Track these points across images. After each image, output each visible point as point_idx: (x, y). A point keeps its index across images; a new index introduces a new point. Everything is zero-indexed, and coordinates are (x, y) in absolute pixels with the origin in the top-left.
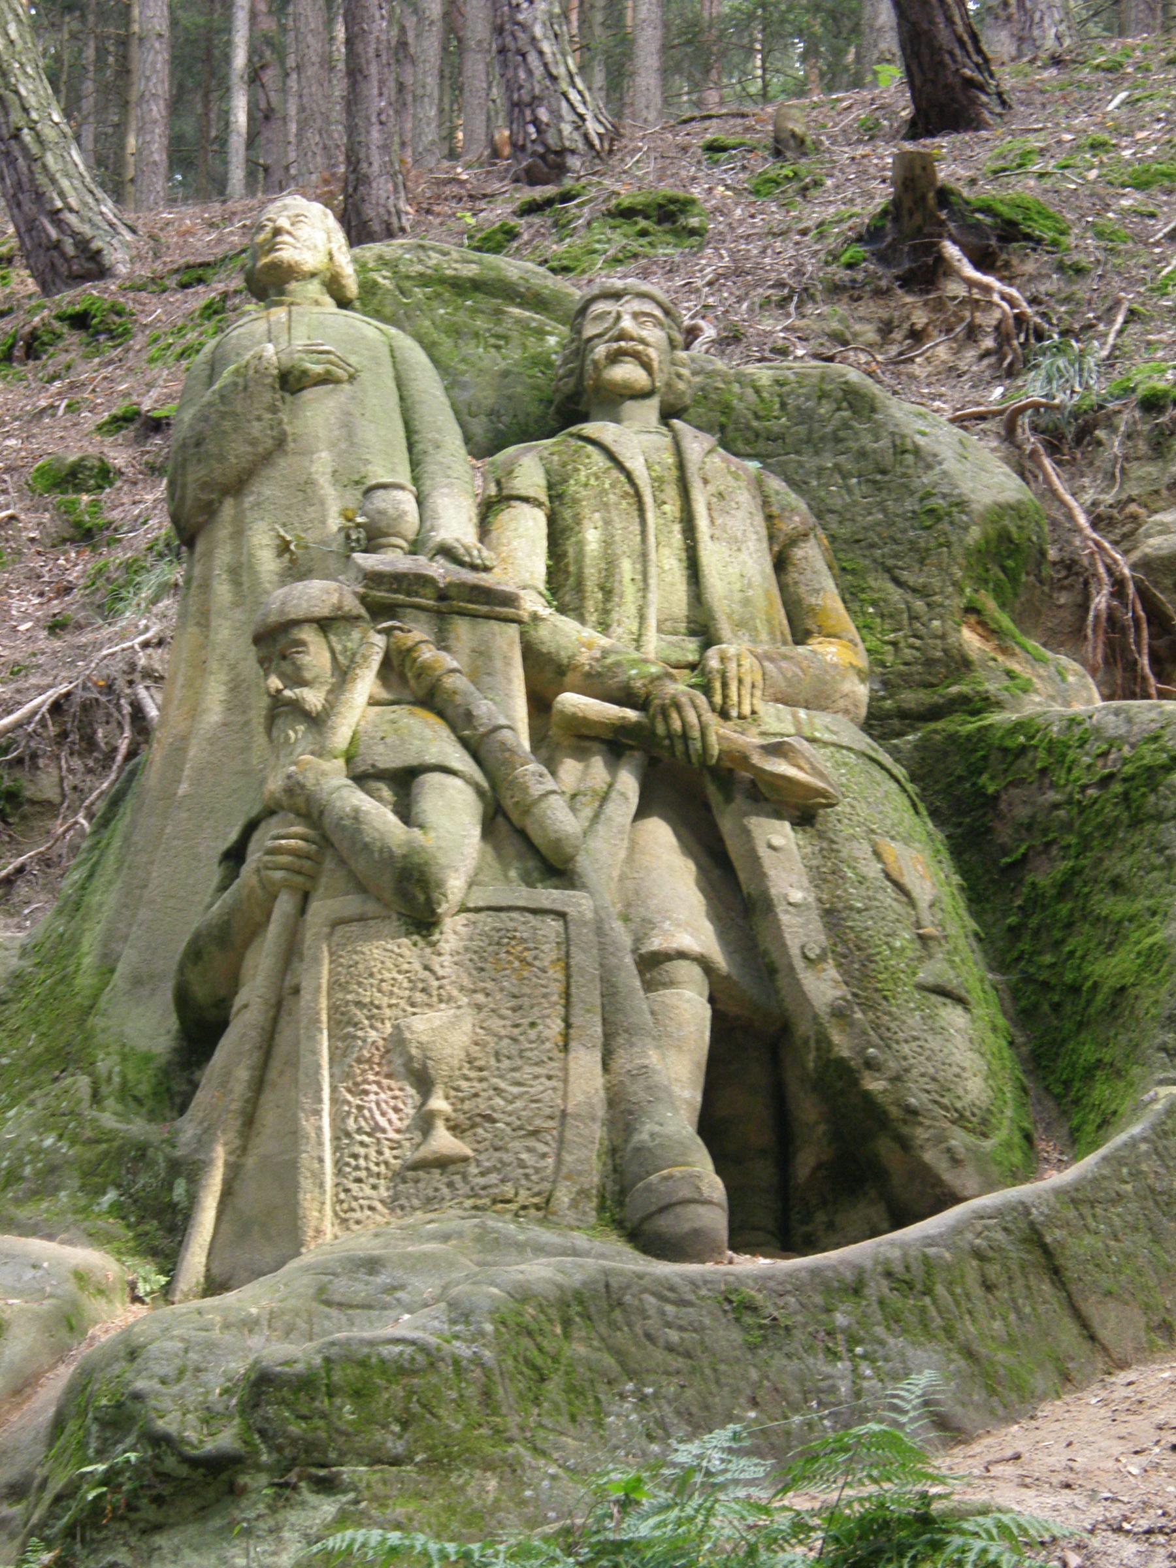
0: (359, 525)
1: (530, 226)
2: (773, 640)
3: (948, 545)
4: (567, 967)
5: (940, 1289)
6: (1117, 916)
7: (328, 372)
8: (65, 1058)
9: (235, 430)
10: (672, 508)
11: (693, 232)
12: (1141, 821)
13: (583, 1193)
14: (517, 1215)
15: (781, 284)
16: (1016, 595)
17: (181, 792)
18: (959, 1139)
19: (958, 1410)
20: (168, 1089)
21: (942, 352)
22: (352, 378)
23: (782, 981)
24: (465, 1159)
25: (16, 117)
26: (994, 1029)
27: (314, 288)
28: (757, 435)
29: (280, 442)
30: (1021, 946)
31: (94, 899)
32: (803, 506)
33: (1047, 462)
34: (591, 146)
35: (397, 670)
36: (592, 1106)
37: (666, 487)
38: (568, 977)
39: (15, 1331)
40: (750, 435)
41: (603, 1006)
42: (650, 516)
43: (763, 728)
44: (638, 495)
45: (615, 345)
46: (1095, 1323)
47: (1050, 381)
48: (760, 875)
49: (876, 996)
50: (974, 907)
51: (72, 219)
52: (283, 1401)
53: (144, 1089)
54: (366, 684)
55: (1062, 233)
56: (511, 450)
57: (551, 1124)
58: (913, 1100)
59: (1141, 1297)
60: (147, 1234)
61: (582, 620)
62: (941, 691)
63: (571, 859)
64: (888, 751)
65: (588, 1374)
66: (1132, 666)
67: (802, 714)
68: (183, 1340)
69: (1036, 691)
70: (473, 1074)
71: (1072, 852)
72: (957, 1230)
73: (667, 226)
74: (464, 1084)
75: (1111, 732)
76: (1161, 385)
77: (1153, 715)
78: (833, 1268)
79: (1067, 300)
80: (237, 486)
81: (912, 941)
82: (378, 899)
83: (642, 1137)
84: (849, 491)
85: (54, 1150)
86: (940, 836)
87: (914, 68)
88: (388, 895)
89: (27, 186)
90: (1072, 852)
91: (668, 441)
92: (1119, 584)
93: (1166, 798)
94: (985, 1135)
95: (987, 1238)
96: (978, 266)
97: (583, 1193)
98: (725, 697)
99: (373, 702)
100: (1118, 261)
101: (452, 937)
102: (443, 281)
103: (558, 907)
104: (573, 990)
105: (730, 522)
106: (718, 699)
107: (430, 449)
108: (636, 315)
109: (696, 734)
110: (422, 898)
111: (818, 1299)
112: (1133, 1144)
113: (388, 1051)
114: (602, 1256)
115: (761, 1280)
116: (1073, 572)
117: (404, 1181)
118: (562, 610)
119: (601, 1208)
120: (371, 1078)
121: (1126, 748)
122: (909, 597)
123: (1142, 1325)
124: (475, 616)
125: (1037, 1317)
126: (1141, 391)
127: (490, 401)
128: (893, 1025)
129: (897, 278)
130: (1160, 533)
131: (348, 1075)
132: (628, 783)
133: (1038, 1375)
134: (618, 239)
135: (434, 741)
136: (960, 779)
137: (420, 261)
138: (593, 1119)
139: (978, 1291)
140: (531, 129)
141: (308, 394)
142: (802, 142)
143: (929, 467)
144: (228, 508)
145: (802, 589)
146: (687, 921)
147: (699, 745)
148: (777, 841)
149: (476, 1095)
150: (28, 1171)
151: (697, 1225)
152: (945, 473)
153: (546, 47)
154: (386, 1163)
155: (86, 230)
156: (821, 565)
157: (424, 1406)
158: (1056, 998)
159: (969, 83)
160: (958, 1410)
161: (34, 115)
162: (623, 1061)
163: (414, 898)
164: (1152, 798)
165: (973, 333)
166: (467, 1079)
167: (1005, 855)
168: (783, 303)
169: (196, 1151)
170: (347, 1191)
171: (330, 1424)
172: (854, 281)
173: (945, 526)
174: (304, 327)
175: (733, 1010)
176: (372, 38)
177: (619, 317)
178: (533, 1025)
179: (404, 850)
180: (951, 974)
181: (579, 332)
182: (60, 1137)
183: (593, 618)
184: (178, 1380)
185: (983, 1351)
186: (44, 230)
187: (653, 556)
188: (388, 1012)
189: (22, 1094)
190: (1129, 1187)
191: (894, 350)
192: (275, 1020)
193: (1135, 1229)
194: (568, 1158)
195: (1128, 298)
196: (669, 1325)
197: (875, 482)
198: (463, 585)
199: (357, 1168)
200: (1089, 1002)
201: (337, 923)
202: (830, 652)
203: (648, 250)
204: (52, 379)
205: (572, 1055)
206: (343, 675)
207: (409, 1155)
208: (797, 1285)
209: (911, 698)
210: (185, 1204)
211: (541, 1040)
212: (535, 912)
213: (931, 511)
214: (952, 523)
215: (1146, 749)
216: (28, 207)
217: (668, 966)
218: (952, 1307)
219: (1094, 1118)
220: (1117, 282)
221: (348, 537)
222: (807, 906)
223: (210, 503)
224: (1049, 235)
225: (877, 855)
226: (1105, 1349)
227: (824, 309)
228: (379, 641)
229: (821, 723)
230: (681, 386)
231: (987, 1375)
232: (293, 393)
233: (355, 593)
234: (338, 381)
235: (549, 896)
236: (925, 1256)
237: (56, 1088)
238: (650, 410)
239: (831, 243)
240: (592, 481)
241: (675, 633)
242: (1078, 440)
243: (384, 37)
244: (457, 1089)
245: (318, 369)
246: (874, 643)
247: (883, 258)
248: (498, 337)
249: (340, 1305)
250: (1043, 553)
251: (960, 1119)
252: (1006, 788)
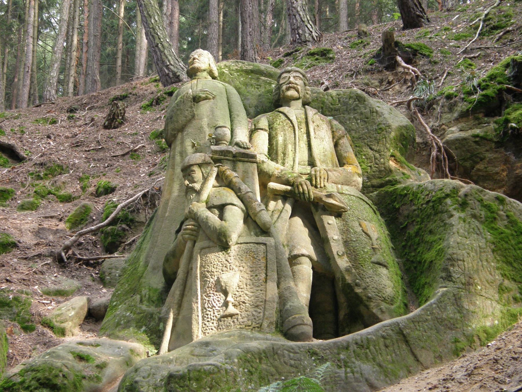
0: (213, 138)
1: (287, 59)
2: (333, 166)
3: (385, 138)
4: (267, 259)
5: (372, 347)
6: (431, 241)
7: (207, 96)
8: (134, 291)
9: (181, 114)
10: (304, 130)
11: (331, 58)
12: (437, 213)
13: (271, 323)
14: (252, 330)
15: (351, 70)
16: (406, 152)
17: (166, 215)
18: (384, 306)
19: (376, 381)
20: (161, 298)
21: (397, 87)
22: (214, 98)
23: (332, 262)
24: (237, 314)
25: (157, 41)
26: (397, 274)
27: (205, 74)
28: (332, 110)
29: (193, 116)
30: (406, 251)
31: (144, 246)
32: (343, 128)
33: (419, 115)
34: (314, 39)
35: (221, 178)
36: (274, 298)
37: (302, 124)
38: (267, 262)
39: (110, 365)
40: (330, 110)
41: (277, 270)
42: (297, 132)
43: (327, 190)
44: (294, 126)
45: (288, 85)
46: (419, 356)
47: (421, 92)
48: (325, 232)
49: (359, 265)
50: (393, 240)
51: (172, 67)
52: (176, 382)
53: (155, 298)
54: (212, 181)
55: (431, 53)
56: (259, 116)
57: (262, 303)
58: (370, 295)
59: (433, 348)
60: (152, 339)
61: (277, 162)
62: (383, 179)
63: (269, 228)
64: (369, 198)
65: (266, 373)
66: (443, 171)
67: (339, 186)
68: (150, 366)
69: (411, 178)
70: (240, 290)
71: (419, 223)
72: (377, 330)
73: (324, 57)
74: (237, 293)
75: (429, 189)
76: (452, 92)
77: (441, 183)
78: (340, 342)
79: (432, 71)
80: (182, 129)
81: (370, 249)
82: (213, 242)
83: (288, 306)
84: (358, 124)
85: (129, 316)
86: (382, 220)
87: (403, 13)
88: (215, 240)
89: (160, 59)
90: (419, 223)
91: (303, 112)
92: (439, 148)
93: (444, 206)
94: (392, 304)
95: (386, 333)
96: (407, 63)
97: (271, 323)
98: (316, 182)
99: (214, 187)
100: (446, 60)
101: (233, 251)
102: (242, 71)
103: (264, 242)
104: (268, 265)
105: (320, 133)
106: (314, 183)
107: (236, 117)
108: (294, 77)
109: (307, 192)
110: (225, 240)
111: (336, 351)
112: (431, 305)
113: (216, 284)
114: (275, 340)
115: (319, 346)
116: (427, 145)
117: (221, 321)
118: (272, 160)
119: (277, 327)
120: (211, 292)
121: (434, 193)
122: (374, 153)
123: (433, 357)
124: (244, 161)
125: (401, 354)
126: (446, 94)
127: (255, 103)
128: (364, 274)
129: (384, 67)
130: (451, 133)
131: (206, 292)
132: (288, 208)
133: (401, 372)
134: (310, 61)
135: (231, 197)
136: (389, 204)
137: (236, 65)
138: (274, 302)
139: (383, 348)
140: (297, 36)
141: (201, 103)
142: (366, 33)
143: (380, 116)
144: (180, 136)
145: (342, 152)
146: (305, 246)
147: (307, 195)
148: (330, 222)
149: (240, 296)
150: (122, 322)
151: (303, 331)
152: (384, 117)
153: (301, 13)
154: (216, 316)
155: (175, 70)
156: (348, 145)
157: (216, 383)
158: (415, 265)
159: (419, 16)
160: (376, 381)
161: (162, 40)
162: (283, 285)
163: (223, 241)
164: (440, 207)
165: (405, 81)
166: (238, 292)
167: (402, 225)
168: (352, 76)
169: (166, 315)
170: (205, 324)
171: (189, 388)
172: (372, 69)
173: (384, 132)
174: (202, 84)
175: (320, 271)
176: (248, 12)
177: (289, 78)
178: (256, 275)
179: (219, 227)
180: (382, 258)
181: (278, 82)
182: (131, 312)
183: (280, 161)
184: (148, 377)
185: (384, 365)
186: (164, 71)
187: (297, 143)
188: (216, 273)
189: (123, 301)
190: (430, 317)
191: (383, 87)
192: (187, 277)
193: (431, 329)
194: (266, 313)
195: (448, 70)
196: (291, 359)
197: (365, 121)
198: (240, 153)
199: (208, 318)
200: (423, 266)
201: (202, 249)
202: (349, 168)
203: (318, 64)
204: (162, 110)
205: (268, 284)
206: (205, 179)
207: (222, 313)
208: (329, 347)
209: (375, 182)
210: (163, 330)
211: (259, 280)
212: (257, 243)
213: (381, 129)
214: (386, 132)
215: (438, 193)
216: (160, 65)
217: (299, 258)
218: (375, 352)
219: (424, 299)
220: (446, 65)
221: (210, 141)
222: (339, 240)
223: (175, 134)
224: (427, 53)
225: (360, 225)
226: (421, 364)
227: (363, 77)
228: (216, 169)
229: (346, 189)
230: (308, 96)
231: (385, 371)
232: (197, 103)
233: (209, 156)
234: (210, 99)
235: (262, 239)
236: (367, 338)
237: (131, 299)
238: (299, 103)
239: (367, 58)
240: (281, 123)
241: (305, 165)
242: (429, 108)
243: (251, 12)
244: (235, 295)
245: (204, 96)
246: (364, 166)
247: (381, 62)
248: (258, 85)
249: (197, 356)
250: (415, 140)
251: (384, 300)
252: (401, 206)
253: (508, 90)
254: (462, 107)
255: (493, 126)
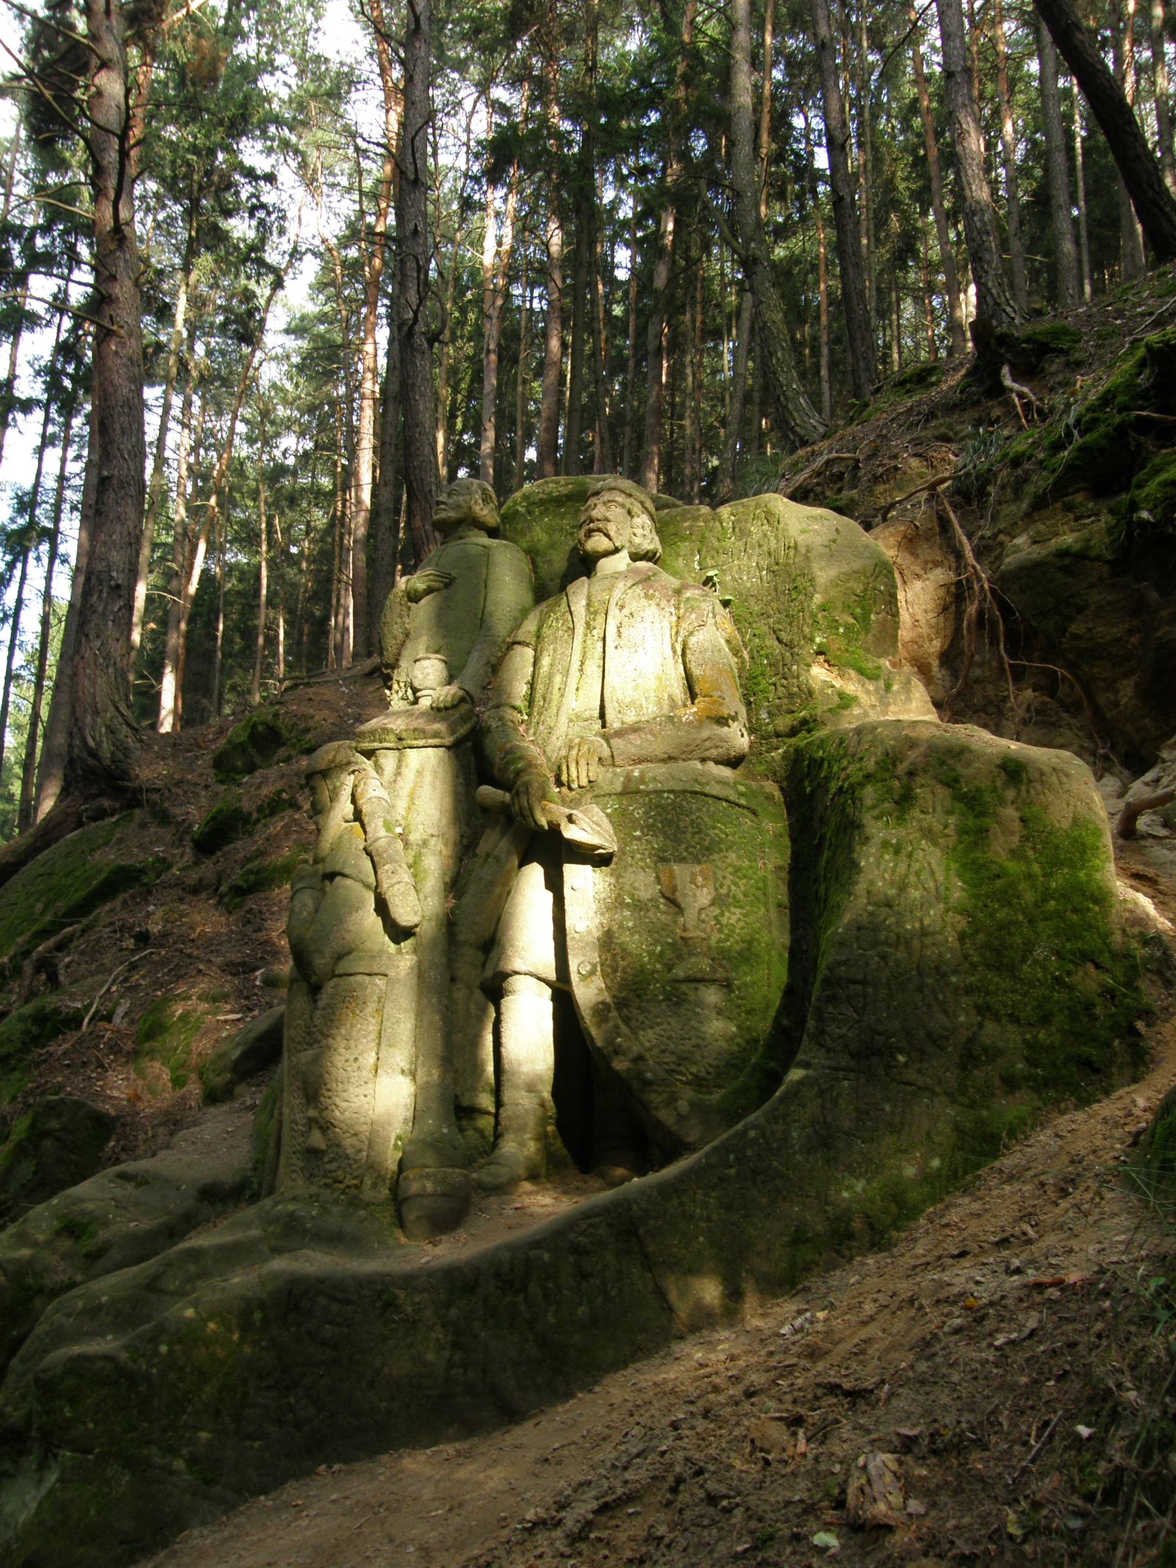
5: (533, 1288)
25: (778, 391)
51: (798, 429)
153: (994, 291)
155: (802, 432)
253: (1142, 425)
254: (1041, 482)
255: (1106, 519)
